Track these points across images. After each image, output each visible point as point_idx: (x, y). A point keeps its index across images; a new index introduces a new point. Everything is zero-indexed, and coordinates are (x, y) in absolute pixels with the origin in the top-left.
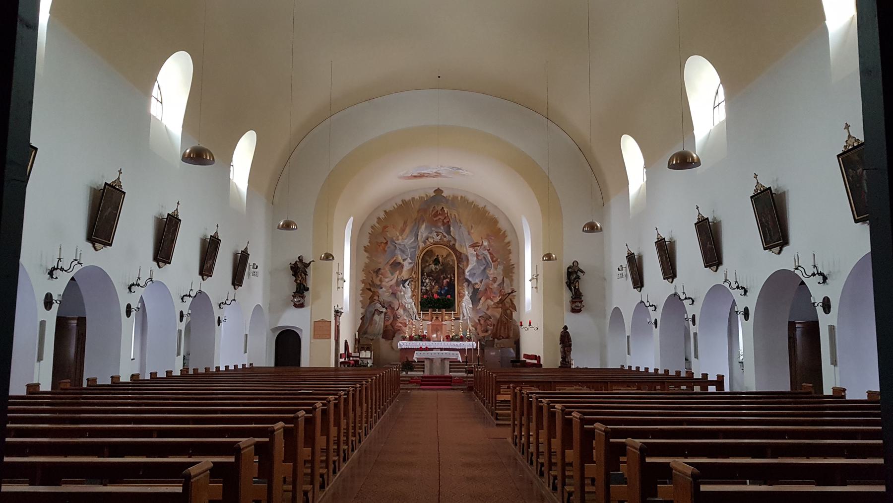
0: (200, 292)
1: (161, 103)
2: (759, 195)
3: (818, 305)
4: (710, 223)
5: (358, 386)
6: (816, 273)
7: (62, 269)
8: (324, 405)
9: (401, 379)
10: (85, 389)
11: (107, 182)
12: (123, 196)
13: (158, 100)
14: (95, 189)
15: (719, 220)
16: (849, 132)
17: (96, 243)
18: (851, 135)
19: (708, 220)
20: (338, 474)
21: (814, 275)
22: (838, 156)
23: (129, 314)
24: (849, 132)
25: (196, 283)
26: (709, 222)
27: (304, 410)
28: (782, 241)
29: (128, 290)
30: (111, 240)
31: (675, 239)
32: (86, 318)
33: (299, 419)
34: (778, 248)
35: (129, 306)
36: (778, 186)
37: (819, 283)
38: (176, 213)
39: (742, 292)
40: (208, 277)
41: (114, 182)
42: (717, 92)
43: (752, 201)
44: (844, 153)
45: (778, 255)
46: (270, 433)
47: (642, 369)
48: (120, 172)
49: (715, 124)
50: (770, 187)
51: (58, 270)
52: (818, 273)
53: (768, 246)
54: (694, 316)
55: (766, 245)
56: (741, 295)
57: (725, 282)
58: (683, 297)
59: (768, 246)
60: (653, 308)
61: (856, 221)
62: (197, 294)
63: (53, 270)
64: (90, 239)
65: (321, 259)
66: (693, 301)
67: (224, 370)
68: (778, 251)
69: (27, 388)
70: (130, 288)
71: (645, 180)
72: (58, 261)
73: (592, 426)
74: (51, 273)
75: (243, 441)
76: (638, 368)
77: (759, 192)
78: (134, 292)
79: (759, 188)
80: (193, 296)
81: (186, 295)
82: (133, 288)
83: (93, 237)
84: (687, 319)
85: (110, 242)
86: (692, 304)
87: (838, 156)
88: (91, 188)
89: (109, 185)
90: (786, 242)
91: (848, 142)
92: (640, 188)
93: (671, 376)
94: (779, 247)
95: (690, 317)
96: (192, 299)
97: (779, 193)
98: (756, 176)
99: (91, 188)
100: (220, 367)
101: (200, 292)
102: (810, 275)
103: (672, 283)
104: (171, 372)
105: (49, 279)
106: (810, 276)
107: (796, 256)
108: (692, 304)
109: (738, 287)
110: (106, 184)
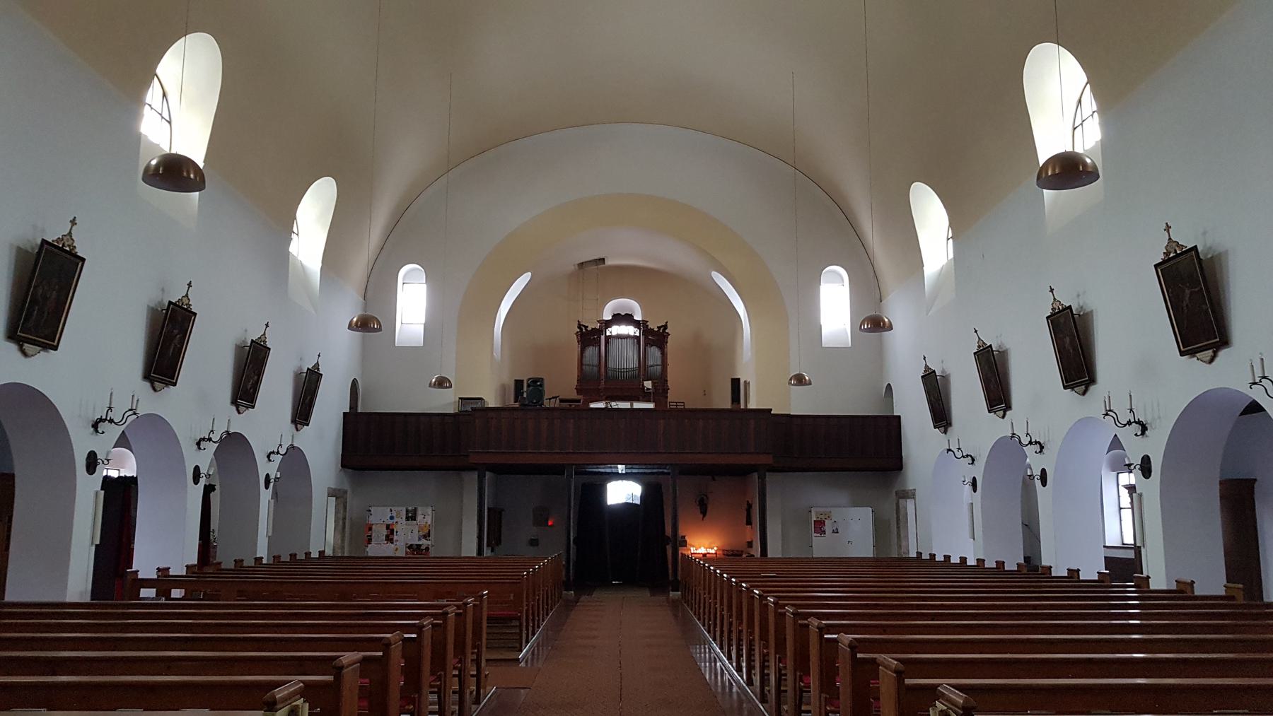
0: (292, 446)
1: (170, 122)
2: (1172, 262)
3: (1135, 467)
4: (938, 377)
5: (525, 573)
6: (1132, 420)
7: (111, 421)
8: (458, 607)
9: (436, 690)
10: (265, 564)
11: (172, 300)
12: (193, 318)
13: (163, 118)
14: (27, 252)
15: (948, 373)
16: (1169, 236)
17: (26, 344)
18: (1172, 238)
19: (992, 349)
20: (542, 627)
21: (1129, 423)
22: (1156, 266)
23: (197, 479)
24: (1169, 236)
25: (228, 419)
26: (993, 351)
27: (455, 605)
28: (1218, 339)
29: (92, 429)
30: (175, 378)
31: (1008, 347)
32: (13, 476)
33: (345, 671)
34: (1210, 353)
35: (197, 469)
36: (1001, 342)
37: (1136, 435)
38: (263, 339)
39: (1037, 448)
40: (247, 408)
41: (259, 338)
42: (1080, 102)
43: (1048, 322)
44: (1164, 262)
45: (1208, 365)
46: (419, 629)
47: (955, 560)
48: (73, 222)
49: (949, 259)
50: (1070, 306)
51: (107, 422)
52: (1135, 422)
53: (1186, 349)
54: (1043, 471)
55: (1184, 348)
56: (1036, 452)
57: (1107, 414)
58: (1025, 440)
59: (1186, 349)
60: (1037, 448)
61: (1182, 354)
62: (287, 449)
63: (99, 422)
64: (147, 376)
65: (430, 385)
66: (1042, 448)
67: (318, 556)
68: (1208, 358)
69: (187, 569)
70: (198, 444)
71: (951, 256)
72: (107, 411)
73: (806, 622)
74: (95, 426)
75: (348, 657)
76: (947, 558)
77: (1172, 255)
78: (205, 449)
79: (1057, 308)
80: (284, 453)
81: (273, 452)
82: (101, 427)
83: (19, 333)
84: (1032, 478)
85: (174, 381)
86: (972, 463)
87: (1156, 266)
88: (19, 249)
89: (174, 304)
90: (1092, 380)
91: (1054, 305)
92: (942, 268)
93: (988, 568)
94: (1083, 387)
95: (1037, 473)
96: (282, 457)
97: (1209, 256)
98: (1168, 228)
99: (19, 249)
100: (310, 553)
101: (292, 446)
102: (1125, 423)
103: (1003, 417)
104: (279, 557)
105: (92, 434)
106: (1125, 425)
107: (1107, 398)
108: (972, 463)
109: (1031, 443)
110: (44, 242)
